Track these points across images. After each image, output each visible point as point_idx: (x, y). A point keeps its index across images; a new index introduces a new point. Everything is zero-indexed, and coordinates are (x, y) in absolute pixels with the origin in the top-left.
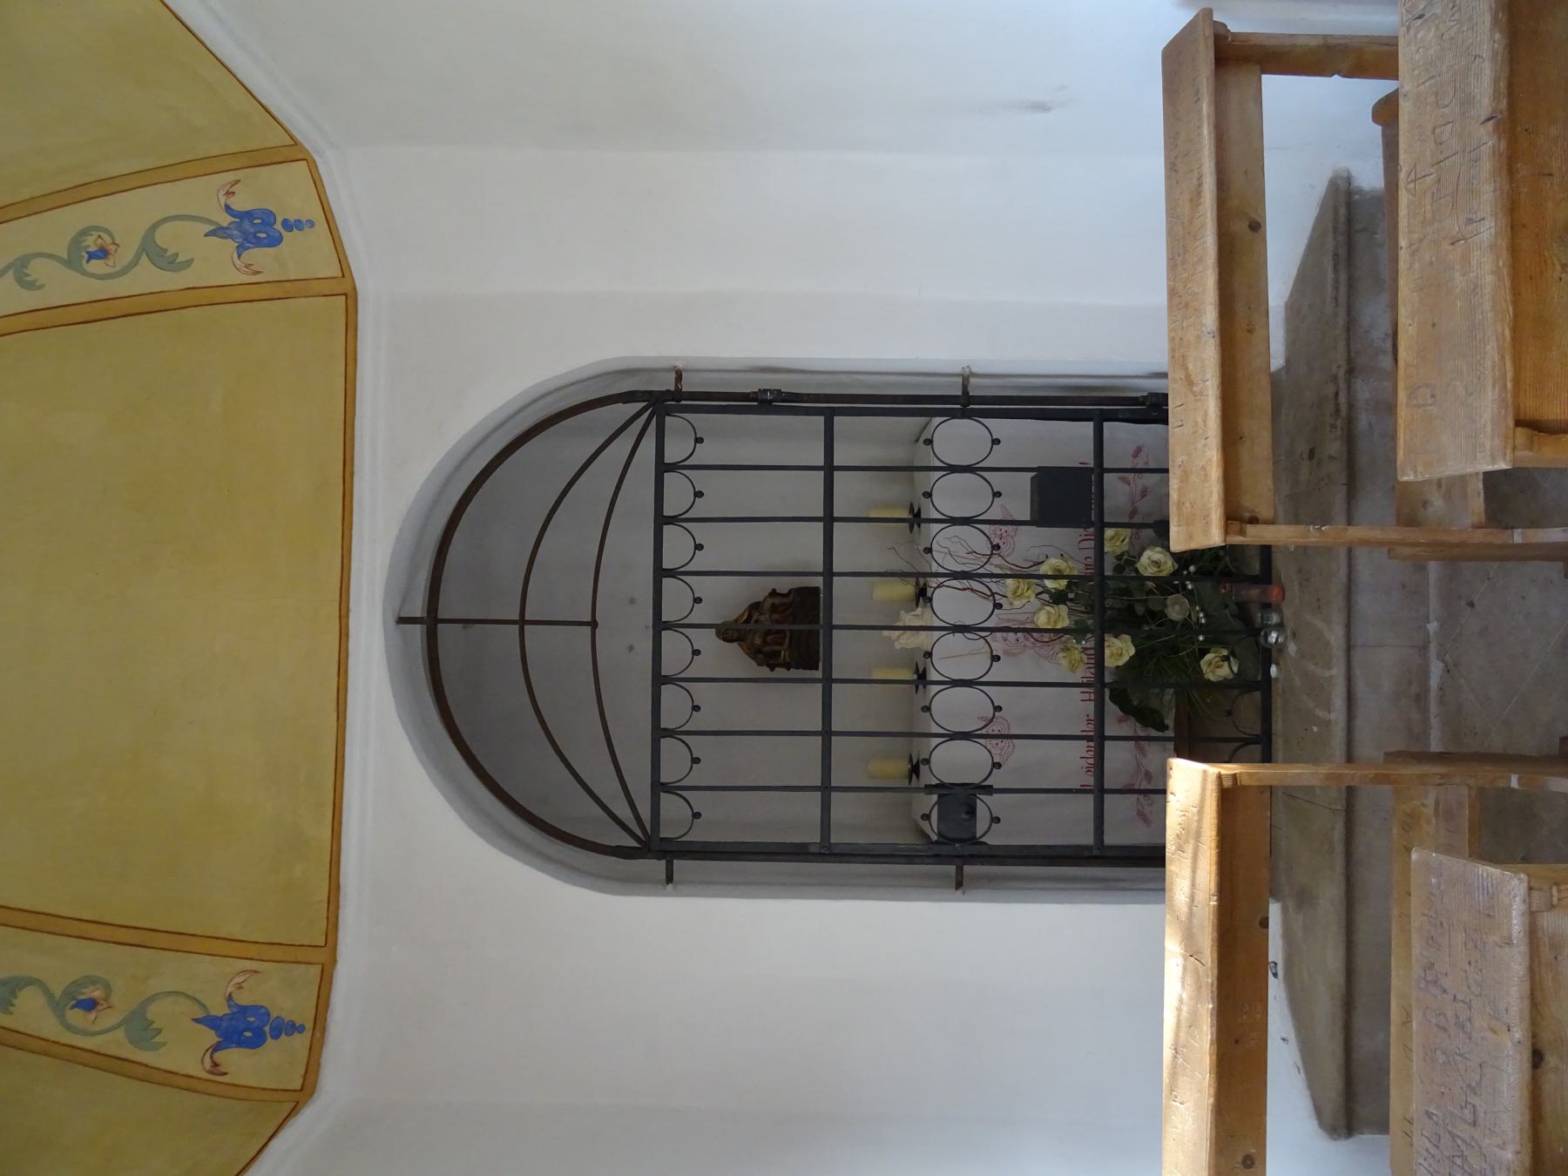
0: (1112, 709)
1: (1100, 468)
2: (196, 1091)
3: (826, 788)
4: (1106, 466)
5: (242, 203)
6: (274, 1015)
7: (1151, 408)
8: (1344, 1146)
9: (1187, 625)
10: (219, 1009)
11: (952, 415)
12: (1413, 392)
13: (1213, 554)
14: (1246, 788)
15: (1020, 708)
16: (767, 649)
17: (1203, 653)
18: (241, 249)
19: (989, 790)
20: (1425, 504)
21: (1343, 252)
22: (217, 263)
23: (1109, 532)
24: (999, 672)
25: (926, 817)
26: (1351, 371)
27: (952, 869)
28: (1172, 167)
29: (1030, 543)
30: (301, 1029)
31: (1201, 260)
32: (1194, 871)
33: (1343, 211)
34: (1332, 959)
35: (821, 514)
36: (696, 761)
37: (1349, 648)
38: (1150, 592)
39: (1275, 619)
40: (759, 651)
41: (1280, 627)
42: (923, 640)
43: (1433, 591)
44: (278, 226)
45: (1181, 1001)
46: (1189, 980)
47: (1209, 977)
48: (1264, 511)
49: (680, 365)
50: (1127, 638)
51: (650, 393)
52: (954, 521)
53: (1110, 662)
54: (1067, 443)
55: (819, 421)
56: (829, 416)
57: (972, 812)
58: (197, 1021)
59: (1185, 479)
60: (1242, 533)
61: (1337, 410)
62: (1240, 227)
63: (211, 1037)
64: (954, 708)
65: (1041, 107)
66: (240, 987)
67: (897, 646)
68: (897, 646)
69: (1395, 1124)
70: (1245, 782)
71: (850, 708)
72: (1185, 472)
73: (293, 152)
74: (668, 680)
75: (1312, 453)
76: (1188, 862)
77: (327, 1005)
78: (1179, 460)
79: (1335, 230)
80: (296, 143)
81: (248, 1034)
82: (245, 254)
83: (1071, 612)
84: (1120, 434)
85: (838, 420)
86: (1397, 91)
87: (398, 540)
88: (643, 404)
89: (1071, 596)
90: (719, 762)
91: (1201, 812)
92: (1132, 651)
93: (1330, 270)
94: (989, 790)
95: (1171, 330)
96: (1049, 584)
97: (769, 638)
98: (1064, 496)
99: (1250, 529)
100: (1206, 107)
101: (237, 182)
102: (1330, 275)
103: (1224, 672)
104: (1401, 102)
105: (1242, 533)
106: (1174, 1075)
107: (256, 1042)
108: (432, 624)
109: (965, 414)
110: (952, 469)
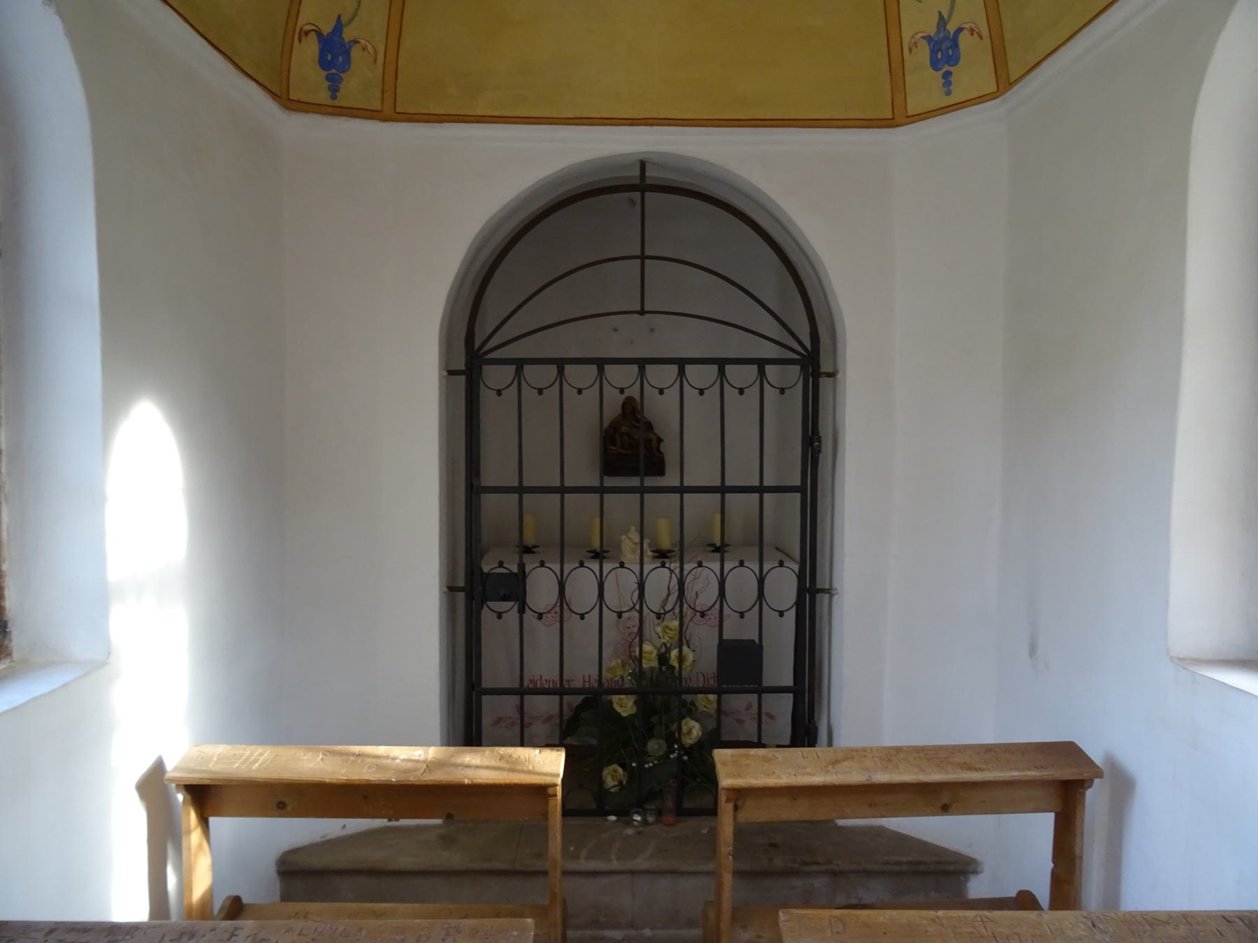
0: (578, 699)
1: (761, 690)
2: (288, 17)
3: (521, 490)
4: (764, 695)
5: (965, 41)
6: (343, 75)
7: (805, 731)
8: (272, 870)
9: (642, 755)
10: (348, 34)
11: (801, 577)
12: (840, 919)
13: (712, 779)
14: (547, 803)
15: (583, 635)
17: (623, 766)
18: (928, 38)
19: (522, 611)
20: (745, 927)
21: (922, 867)
22: (917, 22)
23: (712, 697)
24: (609, 617)
25: (501, 565)
26: (835, 874)
27: (461, 583)
28: (988, 749)
29: (705, 640)
30: (334, 97)
31: (922, 770)
32: (487, 768)
33: (951, 868)
34: (406, 861)
35: (727, 484)
36: (540, 392)
37: (632, 873)
38: (668, 727)
39: (651, 819)
41: (645, 822)
42: (631, 557)
43: (672, 932)
44: (946, 68)
45: (394, 759)
46: (409, 765)
47: (412, 779)
48: (743, 816)
49: (839, 376)
50: (634, 711)
52: (722, 583)
53: (615, 698)
54: (779, 666)
55: (797, 482)
56: (801, 489)
57: (505, 598)
58: (339, 17)
59: (766, 760)
60: (728, 800)
61: (806, 864)
62: (945, 799)
63: (327, 29)
64: (583, 585)
65: (1033, 650)
66: (364, 49)
67: (623, 537)
68: (623, 537)
69: (292, 907)
70: (551, 803)
71: (582, 508)
72: (770, 760)
73: (1004, 83)
74: (601, 371)
75: (774, 846)
76: (493, 763)
78: (777, 755)
79: (939, 863)
80: (1011, 84)
81: (329, 57)
82: (924, 43)
83: (652, 669)
84: (783, 706)
85: (797, 496)
86: (1041, 909)
87: (706, 162)
88: (809, 347)
89: (664, 668)
91: (529, 772)
92: (624, 715)
93: (910, 859)
94: (522, 611)
95: (871, 749)
96: (674, 653)
98: (740, 664)
99: (730, 806)
100: (1032, 774)
101: (981, 38)
102: (904, 859)
103: (610, 782)
104: (1036, 912)
105: (728, 800)
106: (341, 754)
107: (324, 64)
108: (639, 187)
109: (801, 591)
110: (761, 582)
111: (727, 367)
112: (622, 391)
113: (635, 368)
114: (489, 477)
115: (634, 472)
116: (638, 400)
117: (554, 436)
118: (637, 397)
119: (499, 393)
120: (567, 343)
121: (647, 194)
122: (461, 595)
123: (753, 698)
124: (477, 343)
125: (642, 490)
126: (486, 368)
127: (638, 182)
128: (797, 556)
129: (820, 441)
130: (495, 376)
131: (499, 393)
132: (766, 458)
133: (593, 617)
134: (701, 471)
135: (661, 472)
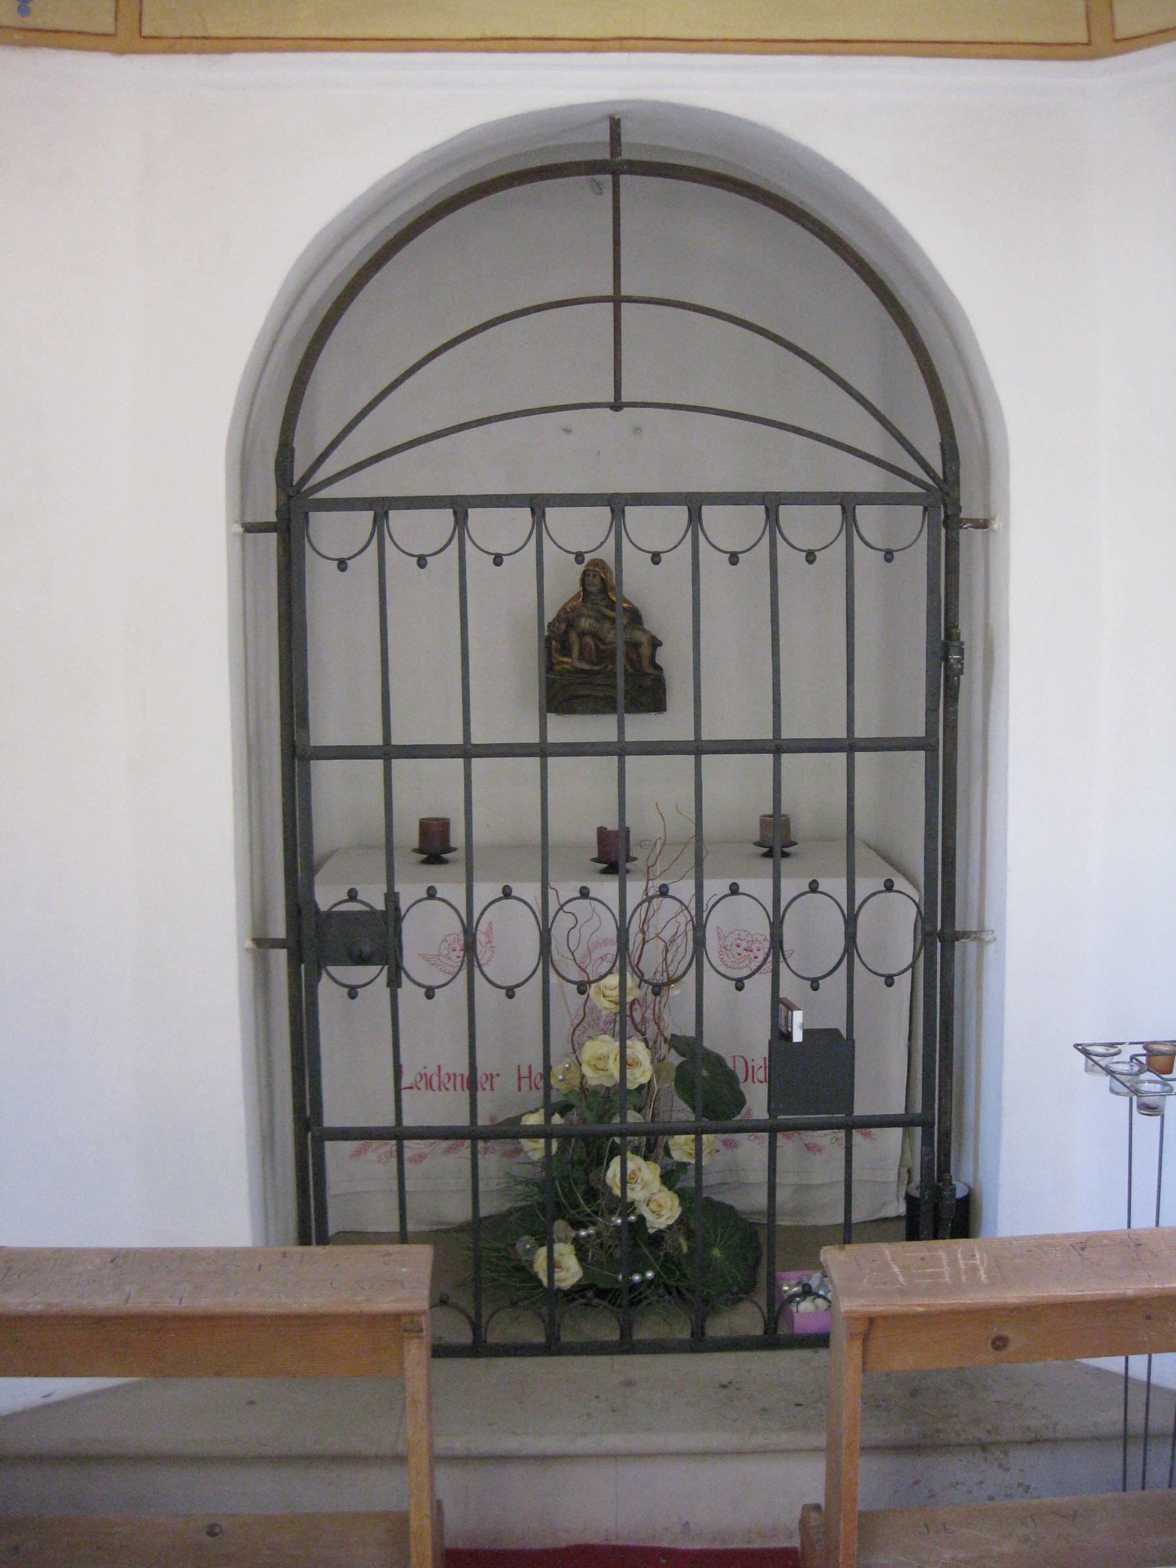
1: (853, 1125)
3: (388, 752)
11: (925, 918)
16: (573, 637)
19: (394, 983)
36: (422, 561)
40: (570, 625)
49: (996, 525)
51: (957, 483)
54: (884, 1076)
56: (925, 744)
57: (362, 960)
74: (538, 516)
77: (59, 46)
88: (938, 469)
90: (422, 604)
94: (394, 983)
97: (589, 640)
110: (851, 920)
111: (783, 510)
112: (579, 557)
113: (682, 512)
114: (326, 730)
115: (605, 705)
116: (611, 564)
117: (446, 643)
118: (611, 562)
119: (342, 565)
120: (470, 467)
121: (624, 179)
122: (280, 957)
123: (829, 1141)
124: (298, 473)
125: (621, 750)
126: (316, 517)
127: (606, 155)
128: (918, 867)
129: (961, 652)
130: (332, 532)
131: (342, 565)
132: (857, 685)
133: (530, 994)
134: (735, 710)
135: (658, 705)
